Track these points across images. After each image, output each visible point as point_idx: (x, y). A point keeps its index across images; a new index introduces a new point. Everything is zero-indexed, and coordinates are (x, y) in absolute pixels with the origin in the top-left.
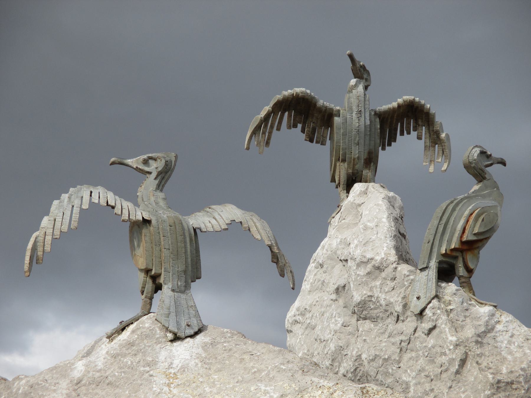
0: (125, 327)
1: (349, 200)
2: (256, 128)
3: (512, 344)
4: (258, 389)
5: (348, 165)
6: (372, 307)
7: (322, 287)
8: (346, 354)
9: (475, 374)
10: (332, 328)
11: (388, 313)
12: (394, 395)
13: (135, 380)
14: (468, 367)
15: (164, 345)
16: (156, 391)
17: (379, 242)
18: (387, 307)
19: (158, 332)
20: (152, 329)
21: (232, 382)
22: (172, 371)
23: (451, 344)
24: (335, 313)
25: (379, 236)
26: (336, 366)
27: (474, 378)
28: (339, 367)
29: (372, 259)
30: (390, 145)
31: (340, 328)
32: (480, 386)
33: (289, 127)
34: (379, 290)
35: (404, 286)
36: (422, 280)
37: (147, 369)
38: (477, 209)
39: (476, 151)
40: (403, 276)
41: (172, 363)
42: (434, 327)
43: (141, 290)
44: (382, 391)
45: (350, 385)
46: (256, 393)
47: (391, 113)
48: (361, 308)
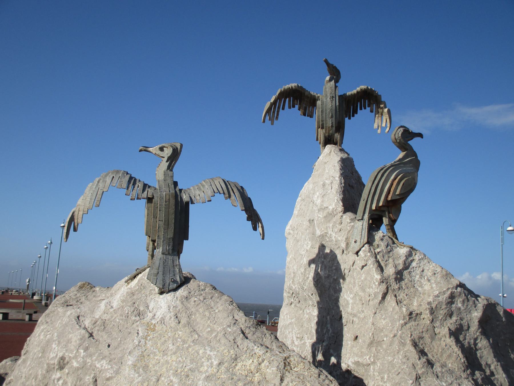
0: (136, 276)
2: (268, 109)
3: (423, 278)
4: (205, 353)
6: (328, 240)
12: (310, 370)
22: (153, 322)
23: (377, 281)
30: (353, 116)
31: (310, 249)
33: (290, 108)
34: (331, 229)
41: (155, 315)
42: (366, 265)
47: (353, 96)
48: (321, 239)
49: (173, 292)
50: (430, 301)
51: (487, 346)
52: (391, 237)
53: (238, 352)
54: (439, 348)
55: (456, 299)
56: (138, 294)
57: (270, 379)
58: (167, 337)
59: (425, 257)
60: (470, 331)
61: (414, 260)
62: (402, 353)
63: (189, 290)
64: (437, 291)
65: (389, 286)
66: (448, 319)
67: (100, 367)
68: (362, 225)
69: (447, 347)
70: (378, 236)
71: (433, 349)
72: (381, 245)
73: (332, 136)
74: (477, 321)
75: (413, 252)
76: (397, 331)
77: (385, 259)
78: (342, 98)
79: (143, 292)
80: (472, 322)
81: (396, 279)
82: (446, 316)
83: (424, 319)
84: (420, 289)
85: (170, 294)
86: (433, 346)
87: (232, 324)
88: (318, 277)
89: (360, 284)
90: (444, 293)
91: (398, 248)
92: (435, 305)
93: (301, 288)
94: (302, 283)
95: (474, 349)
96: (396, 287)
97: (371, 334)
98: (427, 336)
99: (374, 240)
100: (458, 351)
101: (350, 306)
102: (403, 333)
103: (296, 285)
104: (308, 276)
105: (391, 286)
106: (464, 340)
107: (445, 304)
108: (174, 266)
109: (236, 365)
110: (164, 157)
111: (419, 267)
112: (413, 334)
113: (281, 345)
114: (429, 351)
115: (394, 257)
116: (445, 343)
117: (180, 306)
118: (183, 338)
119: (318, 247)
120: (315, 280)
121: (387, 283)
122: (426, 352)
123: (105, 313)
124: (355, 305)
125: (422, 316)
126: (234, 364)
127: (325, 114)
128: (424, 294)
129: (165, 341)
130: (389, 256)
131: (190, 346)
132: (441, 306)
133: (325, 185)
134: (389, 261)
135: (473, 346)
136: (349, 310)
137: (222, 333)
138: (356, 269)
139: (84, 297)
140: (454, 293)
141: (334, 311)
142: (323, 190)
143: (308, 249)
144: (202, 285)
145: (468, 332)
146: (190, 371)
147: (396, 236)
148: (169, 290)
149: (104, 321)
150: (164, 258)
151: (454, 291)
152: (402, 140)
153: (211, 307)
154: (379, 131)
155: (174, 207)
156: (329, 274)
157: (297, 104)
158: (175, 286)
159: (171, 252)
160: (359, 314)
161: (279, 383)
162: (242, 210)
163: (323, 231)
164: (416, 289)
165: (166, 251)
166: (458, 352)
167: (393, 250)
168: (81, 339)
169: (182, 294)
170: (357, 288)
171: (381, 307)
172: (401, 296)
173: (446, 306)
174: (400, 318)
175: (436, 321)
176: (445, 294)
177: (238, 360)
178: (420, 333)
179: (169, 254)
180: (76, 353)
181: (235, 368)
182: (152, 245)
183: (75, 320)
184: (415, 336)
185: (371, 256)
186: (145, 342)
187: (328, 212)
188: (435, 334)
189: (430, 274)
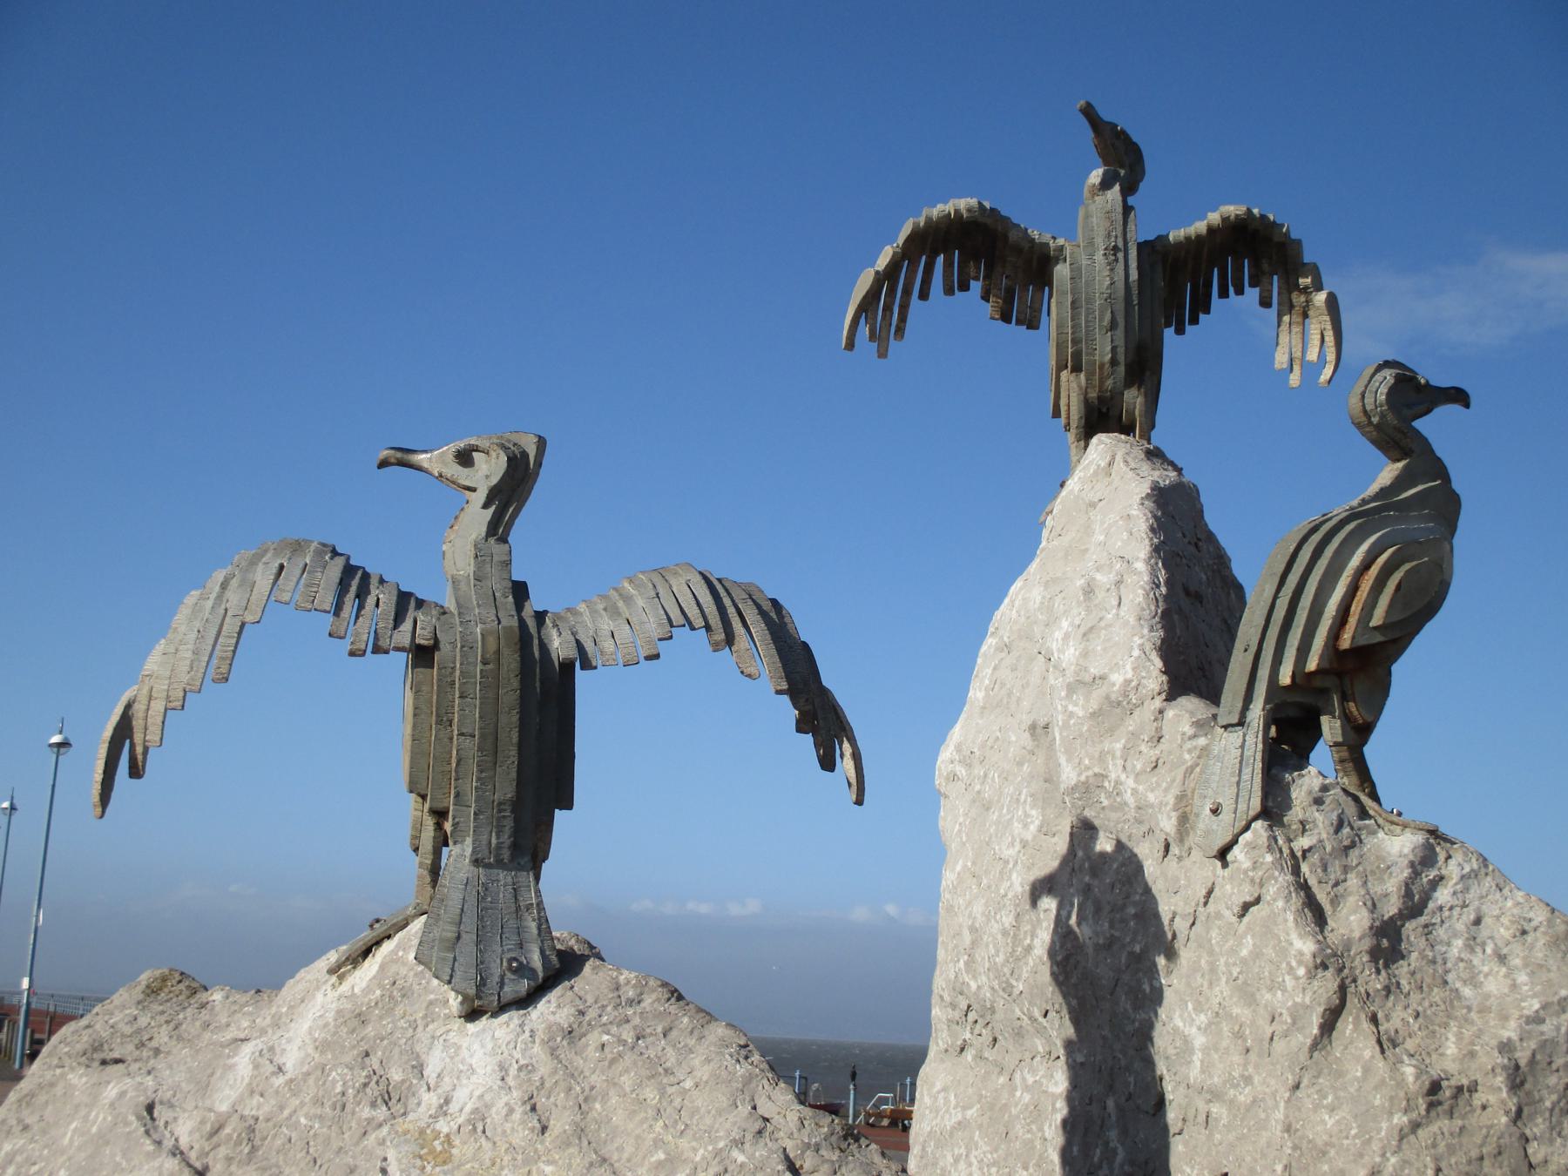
1: (1070, 488)
3: (1478, 949)
5: (1087, 380)
6: (1106, 803)
9: (1367, 1057)
10: (1016, 831)
11: (1145, 828)
14: (1348, 1032)
22: (443, 1126)
23: (1300, 963)
24: (1024, 791)
25: (1122, 614)
26: (1026, 932)
27: (1363, 1067)
28: (1032, 936)
30: (1194, 321)
31: (1035, 837)
32: (1378, 1096)
33: (949, 291)
34: (1120, 762)
37: (381, 1113)
38: (1385, 550)
39: (1385, 378)
40: (1179, 737)
41: (447, 1101)
42: (1258, 901)
43: (413, 844)
47: (1194, 245)
49: (518, 1009)
52: (1352, 790)
56: (381, 1018)
59: (1486, 866)
61: (1442, 878)
63: (578, 1002)
65: (1347, 981)
68: (1242, 747)
73: (1112, 398)
75: (1438, 849)
77: (1332, 877)
78: (1155, 253)
79: (399, 1011)
81: (1375, 954)
83: (1484, 1107)
84: (1467, 992)
85: (504, 1017)
87: (749, 1136)
88: (1069, 946)
89: (1235, 974)
91: (1381, 834)
92: (1528, 1053)
93: (1004, 990)
94: (1006, 970)
99: (1287, 804)
101: (1195, 1058)
102: (1405, 1163)
103: (984, 978)
104: (1028, 941)
105: (1355, 981)
108: (518, 909)
110: (473, 490)
111: (1464, 906)
112: (1443, 1165)
115: (1365, 870)
117: (544, 1067)
119: (1068, 830)
120: (1059, 958)
123: (252, 1092)
125: (1479, 1098)
127: (1087, 317)
128: (1484, 1010)
130: (1345, 866)
133: (1092, 591)
134: (1349, 883)
136: (1194, 1073)
138: (1219, 915)
141: (1131, 1079)
142: (1088, 610)
144: (628, 982)
147: (1373, 785)
150: (483, 879)
152: (1390, 417)
153: (666, 1070)
154: (1295, 379)
156: (1112, 935)
157: (976, 279)
158: (524, 985)
159: (506, 855)
160: (1232, 1092)
162: (779, 692)
163: (1088, 768)
164: (1451, 990)
165: (486, 852)
169: (551, 1018)
170: (1222, 990)
171: (1316, 1063)
172: (1397, 1017)
175: (1532, 1117)
178: (1469, 1162)
179: (499, 864)
183: (139, 1118)
185: (1278, 863)
187: (1107, 697)
188: (1531, 1166)
189: (1504, 933)
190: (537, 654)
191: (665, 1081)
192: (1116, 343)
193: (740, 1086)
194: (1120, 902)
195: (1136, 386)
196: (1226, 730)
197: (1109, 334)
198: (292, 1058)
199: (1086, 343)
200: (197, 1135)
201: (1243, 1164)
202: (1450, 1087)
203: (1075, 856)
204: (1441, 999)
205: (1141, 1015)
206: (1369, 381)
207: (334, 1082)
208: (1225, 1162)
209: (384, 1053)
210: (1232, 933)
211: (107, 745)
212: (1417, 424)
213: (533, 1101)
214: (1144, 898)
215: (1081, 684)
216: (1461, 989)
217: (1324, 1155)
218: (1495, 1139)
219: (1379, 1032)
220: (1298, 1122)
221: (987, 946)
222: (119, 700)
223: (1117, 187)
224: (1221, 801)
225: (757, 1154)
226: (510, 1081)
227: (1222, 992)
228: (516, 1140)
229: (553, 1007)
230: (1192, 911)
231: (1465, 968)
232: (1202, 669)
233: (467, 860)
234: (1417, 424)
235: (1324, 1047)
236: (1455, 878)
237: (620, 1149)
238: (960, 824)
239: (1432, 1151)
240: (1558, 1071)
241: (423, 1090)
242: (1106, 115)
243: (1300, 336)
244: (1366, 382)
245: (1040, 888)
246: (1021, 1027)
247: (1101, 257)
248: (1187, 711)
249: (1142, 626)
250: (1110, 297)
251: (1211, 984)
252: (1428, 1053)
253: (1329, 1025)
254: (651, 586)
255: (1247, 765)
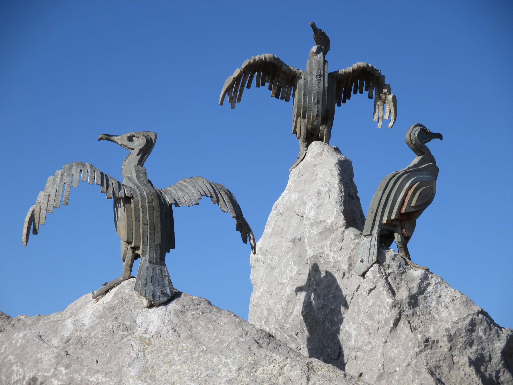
1: (307, 159)
3: (440, 304)
4: (220, 361)
5: (308, 121)
6: (323, 262)
7: (281, 233)
8: (299, 299)
10: (288, 274)
11: (336, 269)
12: (335, 372)
13: (115, 343)
15: (141, 311)
16: (133, 356)
17: (331, 206)
18: (335, 264)
19: (136, 298)
20: (131, 295)
21: (197, 351)
22: (147, 336)
23: (388, 305)
24: (291, 261)
26: (291, 307)
29: (324, 221)
30: (344, 102)
31: (295, 275)
33: (258, 86)
34: (329, 248)
35: (350, 248)
36: (365, 245)
37: (126, 333)
39: (417, 129)
41: (147, 330)
42: (375, 288)
44: (325, 368)
45: (298, 360)
46: (218, 365)
47: (347, 75)
49: (164, 305)
50: (449, 328)
51: (511, 380)
52: (403, 257)
53: (256, 359)
54: (458, 378)
55: (477, 326)
56: (120, 308)
57: (296, 380)
58: (169, 349)
59: (443, 281)
60: (491, 363)
61: (430, 284)
62: (418, 381)
63: (182, 304)
64: (456, 318)
65: (402, 311)
66: (468, 348)
67: (95, 380)
68: (371, 242)
69: (466, 377)
70: (389, 255)
71: (450, 379)
72: (392, 265)
73: (316, 128)
74: (500, 351)
75: (429, 275)
76: (412, 359)
77: (397, 281)
78: (334, 77)
79: (125, 306)
80: (495, 353)
81: (410, 304)
82: (465, 345)
83: (441, 347)
84: (436, 316)
85: (161, 307)
86: (451, 376)
87: (244, 335)
88: (308, 309)
89: (367, 311)
90: (464, 319)
91: (412, 270)
92: (454, 332)
93: (281, 328)
94: (282, 321)
95: (496, 382)
96: (410, 312)
97: (380, 366)
98: (445, 365)
99: (384, 260)
100: (478, 380)
101: (352, 339)
102: (418, 362)
103: (273, 326)
104: (291, 310)
105: (404, 311)
106: (485, 371)
107: (464, 331)
108: (162, 276)
109: (256, 370)
110: (133, 149)
111: (436, 292)
112: (429, 362)
113: (298, 354)
114: (446, 381)
115: (407, 280)
116: (464, 373)
117: (175, 321)
118: (189, 349)
119: (308, 272)
120: (304, 314)
121: (400, 308)
122: (443, 382)
123: (77, 331)
124: (359, 337)
125: (439, 344)
126: (254, 369)
127: (309, 99)
128: (441, 321)
129: (168, 353)
130: (401, 279)
131: (199, 356)
132: (460, 333)
133: (320, 193)
134: (402, 284)
135: (495, 379)
136: (352, 343)
137: (234, 343)
138: (361, 294)
139: (8, 325)
140: (475, 320)
141: (329, 350)
142: (319, 199)
143: (293, 275)
144: (196, 299)
145: (489, 364)
146: (207, 377)
147: (409, 256)
148: (160, 302)
149: (80, 338)
150: (152, 267)
151: (475, 318)
152: (418, 142)
153: (214, 320)
154: (380, 125)
155: (158, 209)
156: (324, 304)
157: (268, 82)
158: (166, 299)
159: (158, 260)
160: (364, 347)
161: (306, 382)
162: (233, 217)
163: (317, 251)
164: (432, 315)
165: (153, 259)
166: (478, 382)
167: (406, 272)
168: (57, 357)
169: (175, 308)
170: (362, 316)
171: (392, 335)
172: (416, 322)
173: (465, 334)
174: (414, 346)
175: (455, 350)
176: (465, 321)
177: (258, 366)
178: (436, 361)
179: (156, 263)
180: (54, 371)
181: (256, 373)
182: (131, 253)
183: (39, 339)
184: (432, 365)
185: (381, 276)
186: (144, 355)
187: (325, 227)
188: (454, 363)
189: (448, 300)
190: (163, 201)
191: (214, 323)
192: (319, 109)
193: (238, 323)
194: (327, 294)
195: (325, 125)
196: (365, 237)
197: (316, 105)
198: (87, 321)
199: (308, 108)
200: (61, 343)
201: (368, 368)
202: (431, 341)
203: (310, 280)
204: (429, 318)
205: (334, 328)
206: (412, 130)
207: (109, 325)
208: (361, 369)
209: (122, 318)
210: (366, 299)
211: (27, 223)
212: (427, 144)
213: (174, 329)
214: (335, 292)
215: (315, 223)
216: (435, 315)
217: (394, 361)
218: (444, 355)
219: (411, 326)
220: (386, 352)
221: (275, 313)
222: (29, 209)
223: (322, 53)
224: (363, 258)
225: (247, 339)
226: (166, 324)
227: (362, 317)
228: (171, 339)
229: (175, 305)
230: (352, 294)
231: (436, 310)
232: (354, 221)
233: (147, 261)
234: (427, 144)
235: (394, 330)
236: (434, 284)
237: (204, 340)
238: (261, 276)
239: (426, 358)
240: (462, 337)
241: (137, 327)
242: (318, 26)
243: (382, 110)
244: (411, 130)
245: (299, 289)
246: (286, 340)
247: (315, 78)
248: (352, 231)
249: (337, 205)
250: (318, 92)
251: (358, 315)
252: (425, 332)
253: (396, 324)
254: (192, 183)
255: (372, 247)
